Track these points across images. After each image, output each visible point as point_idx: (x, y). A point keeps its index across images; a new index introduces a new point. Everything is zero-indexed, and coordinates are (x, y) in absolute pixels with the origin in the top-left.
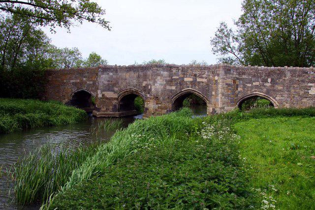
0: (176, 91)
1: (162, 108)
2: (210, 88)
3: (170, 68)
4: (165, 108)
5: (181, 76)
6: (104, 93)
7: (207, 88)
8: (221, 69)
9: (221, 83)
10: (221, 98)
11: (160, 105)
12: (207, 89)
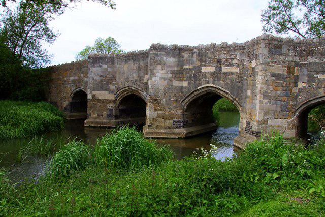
0: (189, 90)
1: (163, 117)
2: (245, 83)
3: (177, 51)
4: (171, 117)
5: (197, 63)
6: (94, 93)
7: (239, 84)
8: (262, 45)
9: (260, 73)
10: (261, 102)
11: (161, 112)
12: (239, 85)
